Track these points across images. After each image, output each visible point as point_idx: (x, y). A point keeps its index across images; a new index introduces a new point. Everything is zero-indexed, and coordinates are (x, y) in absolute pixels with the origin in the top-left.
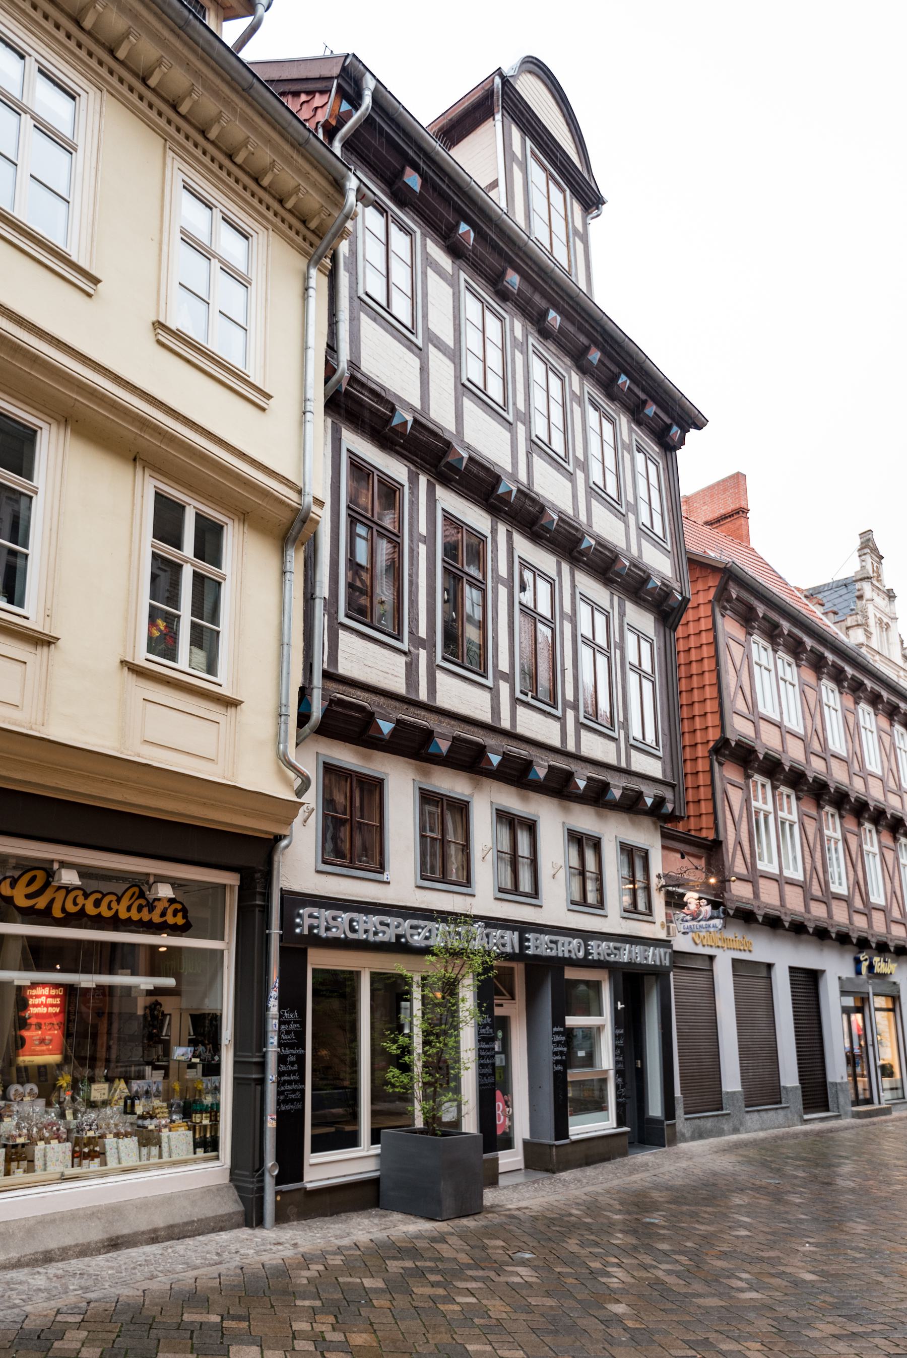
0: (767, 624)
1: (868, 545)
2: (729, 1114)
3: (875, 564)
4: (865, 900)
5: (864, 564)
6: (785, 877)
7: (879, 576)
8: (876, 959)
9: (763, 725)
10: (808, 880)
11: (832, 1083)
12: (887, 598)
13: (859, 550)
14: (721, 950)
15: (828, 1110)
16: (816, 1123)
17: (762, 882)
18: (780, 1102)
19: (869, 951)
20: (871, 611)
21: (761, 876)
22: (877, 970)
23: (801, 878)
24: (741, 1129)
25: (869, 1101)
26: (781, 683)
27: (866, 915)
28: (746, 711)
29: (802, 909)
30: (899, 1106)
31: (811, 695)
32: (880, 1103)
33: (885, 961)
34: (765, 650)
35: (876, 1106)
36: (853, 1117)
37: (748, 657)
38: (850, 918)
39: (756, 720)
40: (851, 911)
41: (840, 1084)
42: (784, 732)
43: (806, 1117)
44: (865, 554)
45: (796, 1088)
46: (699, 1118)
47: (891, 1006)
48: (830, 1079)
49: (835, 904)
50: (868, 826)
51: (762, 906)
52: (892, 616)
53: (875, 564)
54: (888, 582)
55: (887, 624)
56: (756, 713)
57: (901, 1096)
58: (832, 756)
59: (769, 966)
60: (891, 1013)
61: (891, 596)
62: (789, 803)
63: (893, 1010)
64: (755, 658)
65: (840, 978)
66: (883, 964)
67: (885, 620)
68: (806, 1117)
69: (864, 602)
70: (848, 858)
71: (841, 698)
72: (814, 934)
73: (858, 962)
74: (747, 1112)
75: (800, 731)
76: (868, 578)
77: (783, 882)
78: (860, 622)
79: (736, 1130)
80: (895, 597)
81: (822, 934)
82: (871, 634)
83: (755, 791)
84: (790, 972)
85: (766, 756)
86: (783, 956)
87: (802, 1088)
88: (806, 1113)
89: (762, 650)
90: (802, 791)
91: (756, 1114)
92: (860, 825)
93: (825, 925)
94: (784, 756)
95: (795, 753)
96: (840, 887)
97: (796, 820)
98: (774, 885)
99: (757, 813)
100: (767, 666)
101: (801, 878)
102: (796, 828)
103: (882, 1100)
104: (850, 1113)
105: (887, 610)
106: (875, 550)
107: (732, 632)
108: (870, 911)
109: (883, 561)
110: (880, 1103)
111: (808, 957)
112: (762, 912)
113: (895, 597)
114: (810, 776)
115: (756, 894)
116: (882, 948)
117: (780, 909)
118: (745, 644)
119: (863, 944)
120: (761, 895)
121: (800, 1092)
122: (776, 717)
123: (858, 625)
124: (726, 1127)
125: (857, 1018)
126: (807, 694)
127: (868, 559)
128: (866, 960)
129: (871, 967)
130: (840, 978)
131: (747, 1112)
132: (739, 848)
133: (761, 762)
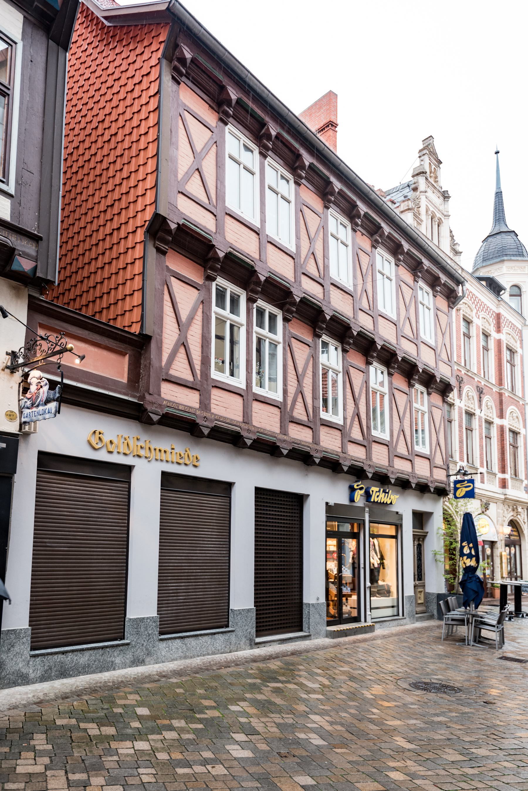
0: (347, 204)
1: (428, 149)
2: (128, 644)
3: (433, 167)
4: (366, 432)
5: (422, 163)
6: (255, 394)
7: (436, 177)
8: (375, 489)
9: (422, 347)
10: (289, 402)
11: (306, 604)
12: (442, 198)
13: (420, 151)
14: (143, 461)
15: (301, 630)
16: (275, 645)
17: (375, 446)
18: (227, 626)
19: (366, 481)
20: (423, 203)
21: (375, 441)
22: (374, 498)
23: (341, 422)
24: (148, 660)
25: (357, 619)
26: (420, 306)
27: (365, 446)
28: (206, 201)
29: (277, 430)
30: (388, 623)
31: (313, 221)
32: (365, 621)
33: (384, 492)
34: (428, 294)
35: (362, 624)
36: (327, 636)
37: (324, 228)
38: (343, 447)
39: (219, 213)
40: (346, 441)
41: (313, 605)
42: (264, 241)
43: (258, 640)
44: (424, 155)
45: (249, 610)
46: (63, 653)
47: (394, 534)
48: (305, 600)
49: (376, 448)
50: (419, 387)
51: (395, 471)
52: (445, 213)
53: (433, 167)
54: (445, 184)
55: (440, 219)
56: (419, 338)
57: (396, 614)
58: (332, 284)
59: (228, 486)
60: (394, 540)
61: (445, 196)
62: (422, 398)
63: (395, 537)
64: (420, 298)
65: (327, 503)
66: (382, 495)
67: (438, 215)
68: (258, 640)
69: (418, 192)
70: (348, 390)
71: (434, 301)
72: (372, 479)
73: (352, 490)
74: (161, 640)
75: (393, 316)
76: (423, 173)
77: (251, 398)
78: (410, 207)
79: (137, 662)
80: (449, 197)
81: (302, 458)
82: (422, 221)
83: (416, 395)
84: (256, 493)
85: (424, 371)
86: (247, 477)
87: (257, 610)
88: (257, 636)
89: (425, 294)
90: (393, 368)
91: (178, 641)
92: (411, 385)
93: (385, 471)
94: (258, 263)
95: (280, 267)
96: (381, 433)
97: (427, 410)
98: (238, 401)
99: (375, 393)
100: (428, 305)
101: (341, 422)
102: (280, 348)
103: (368, 618)
104: (323, 632)
105: (441, 208)
106: (433, 154)
107: (187, 103)
108: (369, 443)
109: (441, 166)
110: (365, 621)
111: (285, 479)
112: (371, 470)
113: (449, 197)
114: (379, 343)
115: (205, 404)
116: (382, 479)
117: (243, 425)
118: (322, 216)
119: (357, 472)
120: (212, 406)
121: (254, 615)
122: (256, 223)
123: (409, 209)
124: (118, 660)
125: (351, 544)
126: (439, 317)
127: (426, 158)
128: (361, 489)
129: (368, 495)
130: (327, 503)
131: (161, 640)
132: (356, 419)
133: (379, 351)
